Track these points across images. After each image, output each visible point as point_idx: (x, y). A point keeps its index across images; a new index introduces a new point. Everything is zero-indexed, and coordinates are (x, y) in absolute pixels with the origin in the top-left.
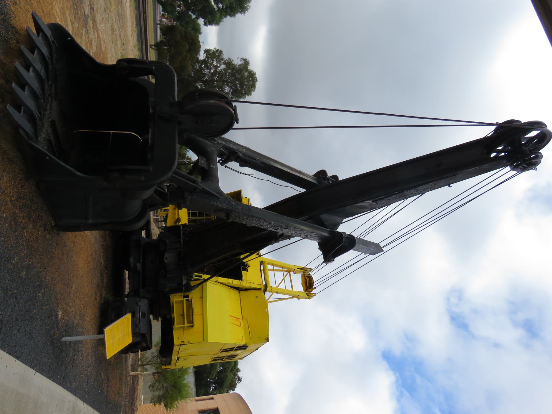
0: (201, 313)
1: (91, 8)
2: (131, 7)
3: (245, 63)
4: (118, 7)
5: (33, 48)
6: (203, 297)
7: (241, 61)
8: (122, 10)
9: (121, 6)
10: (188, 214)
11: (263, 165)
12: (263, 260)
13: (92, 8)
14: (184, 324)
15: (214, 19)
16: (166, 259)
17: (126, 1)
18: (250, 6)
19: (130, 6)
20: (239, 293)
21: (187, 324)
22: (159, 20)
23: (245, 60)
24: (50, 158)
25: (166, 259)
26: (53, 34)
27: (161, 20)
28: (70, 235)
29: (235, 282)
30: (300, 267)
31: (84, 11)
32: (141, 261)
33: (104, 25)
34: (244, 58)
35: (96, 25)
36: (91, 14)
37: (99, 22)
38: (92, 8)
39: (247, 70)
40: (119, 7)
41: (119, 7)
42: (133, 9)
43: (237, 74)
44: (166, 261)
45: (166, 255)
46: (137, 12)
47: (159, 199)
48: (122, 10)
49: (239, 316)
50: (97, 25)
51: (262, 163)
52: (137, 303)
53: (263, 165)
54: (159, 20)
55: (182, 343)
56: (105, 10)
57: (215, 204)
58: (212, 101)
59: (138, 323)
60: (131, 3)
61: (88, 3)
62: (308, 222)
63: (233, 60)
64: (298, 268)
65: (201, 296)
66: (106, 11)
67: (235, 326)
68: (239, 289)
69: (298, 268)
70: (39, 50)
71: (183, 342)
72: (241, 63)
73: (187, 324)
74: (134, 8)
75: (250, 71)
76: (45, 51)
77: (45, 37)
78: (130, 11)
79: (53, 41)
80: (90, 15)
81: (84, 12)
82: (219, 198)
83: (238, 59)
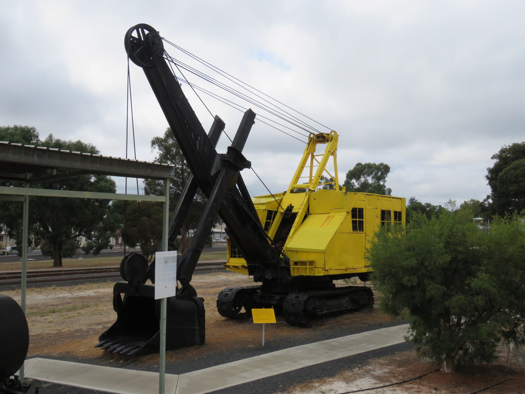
0: (307, 253)
1: (98, 324)
2: (104, 287)
3: (157, 143)
4: (104, 301)
5: (108, 347)
6: (297, 251)
7: (155, 148)
8: (106, 297)
9: (103, 298)
10: (240, 258)
11: (177, 220)
12: (290, 189)
13: (99, 324)
14: (306, 268)
15: (107, 189)
16: (269, 277)
17: (99, 292)
18: (90, 144)
19: (104, 288)
20: (311, 214)
21: (307, 266)
22: (120, 248)
23: (153, 143)
24: (150, 341)
25: (269, 277)
26: (104, 340)
27: (120, 244)
28: (207, 338)
29: (297, 220)
30: (307, 146)
31: (100, 329)
32: (274, 295)
33: (111, 316)
34: (151, 144)
35: (111, 321)
36: (103, 324)
37: (109, 319)
38: (99, 324)
39: (165, 140)
40: (103, 300)
41: (103, 300)
42: (106, 284)
43: (172, 153)
44: (270, 278)
45: (267, 278)
46: (109, 279)
47: (185, 292)
48: (106, 297)
49: (327, 216)
50: (110, 320)
51: (175, 221)
52: (287, 301)
53: (177, 220)
54: (120, 248)
55: (324, 269)
56: (100, 315)
57: (188, 260)
58: (125, 267)
59: (299, 301)
60: (100, 286)
61: (95, 326)
62: (223, 176)
63: (156, 158)
64: (307, 150)
65: (296, 252)
66: (101, 314)
67: (389, 198)
68: (306, 217)
69: (307, 150)
70: (110, 345)
71: (323, 268)
72: (157, 148)
73: (307, 266)
74: (105, 284)
75: (166, 135)
76: (110, 343)
77: (105, 343)
78: (108, 288)
79: (107, 340)
80: (103, 326)
81: (101, 328)
82: (186, 257)
83: (153, 152)
